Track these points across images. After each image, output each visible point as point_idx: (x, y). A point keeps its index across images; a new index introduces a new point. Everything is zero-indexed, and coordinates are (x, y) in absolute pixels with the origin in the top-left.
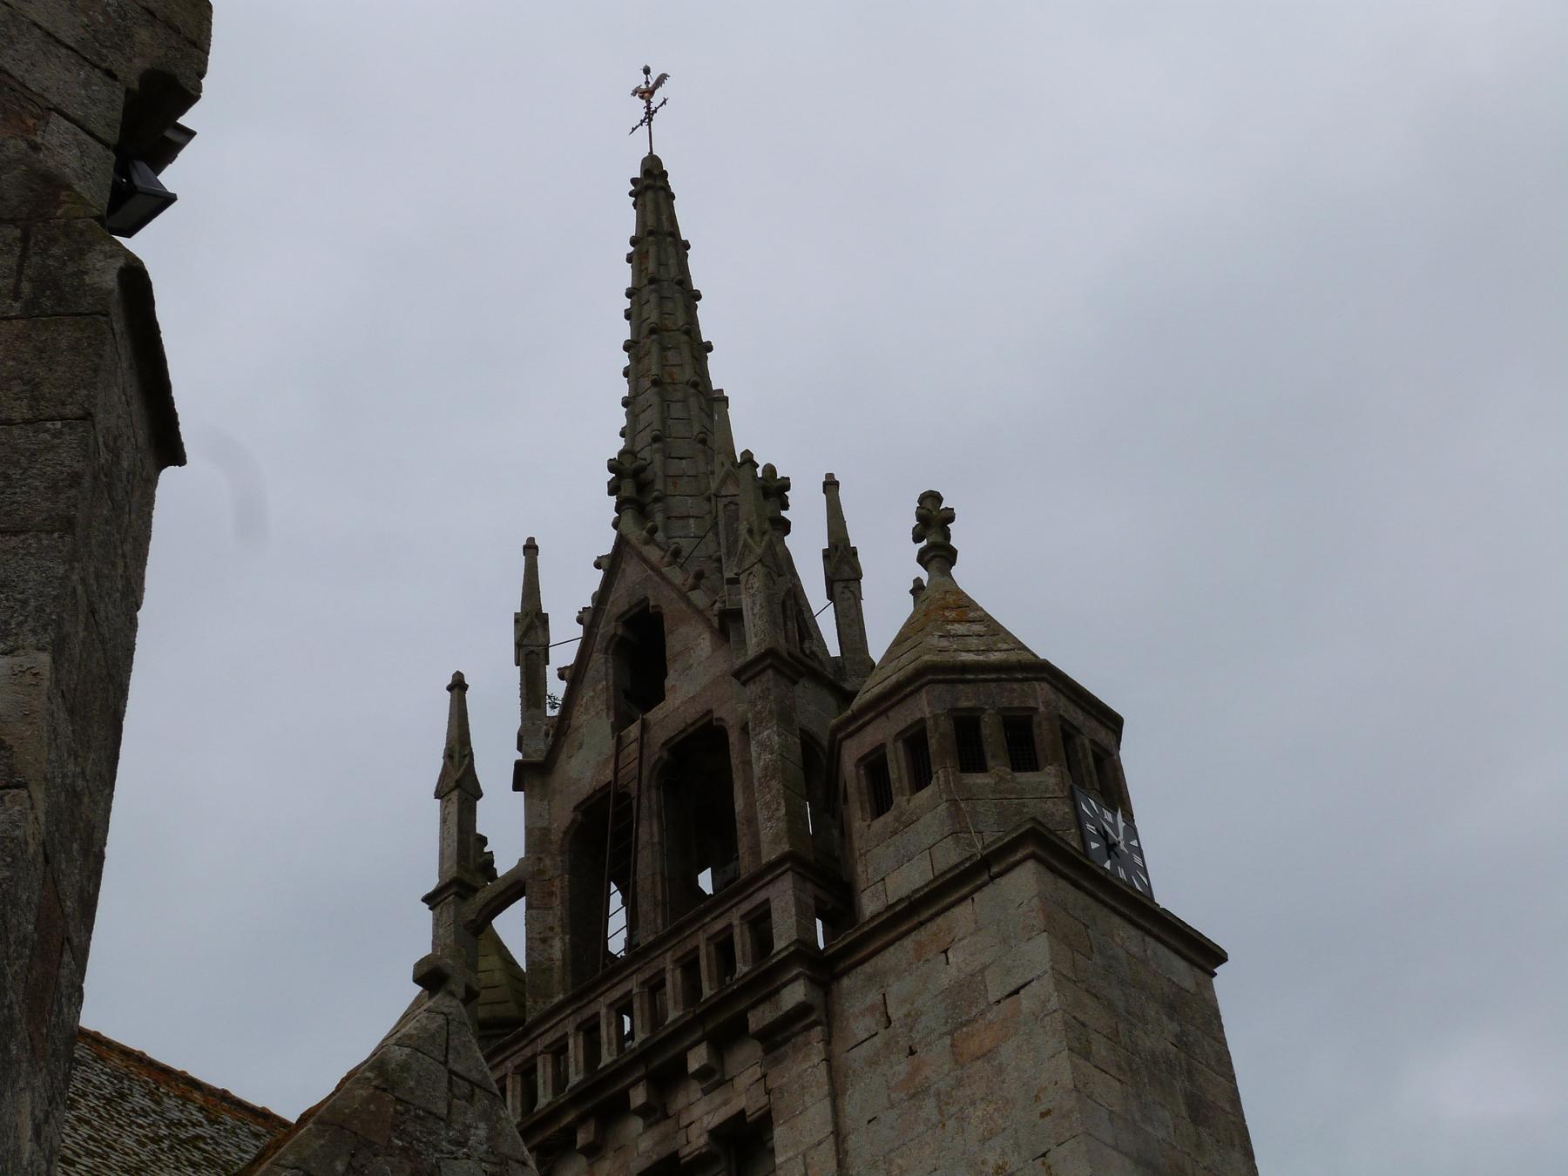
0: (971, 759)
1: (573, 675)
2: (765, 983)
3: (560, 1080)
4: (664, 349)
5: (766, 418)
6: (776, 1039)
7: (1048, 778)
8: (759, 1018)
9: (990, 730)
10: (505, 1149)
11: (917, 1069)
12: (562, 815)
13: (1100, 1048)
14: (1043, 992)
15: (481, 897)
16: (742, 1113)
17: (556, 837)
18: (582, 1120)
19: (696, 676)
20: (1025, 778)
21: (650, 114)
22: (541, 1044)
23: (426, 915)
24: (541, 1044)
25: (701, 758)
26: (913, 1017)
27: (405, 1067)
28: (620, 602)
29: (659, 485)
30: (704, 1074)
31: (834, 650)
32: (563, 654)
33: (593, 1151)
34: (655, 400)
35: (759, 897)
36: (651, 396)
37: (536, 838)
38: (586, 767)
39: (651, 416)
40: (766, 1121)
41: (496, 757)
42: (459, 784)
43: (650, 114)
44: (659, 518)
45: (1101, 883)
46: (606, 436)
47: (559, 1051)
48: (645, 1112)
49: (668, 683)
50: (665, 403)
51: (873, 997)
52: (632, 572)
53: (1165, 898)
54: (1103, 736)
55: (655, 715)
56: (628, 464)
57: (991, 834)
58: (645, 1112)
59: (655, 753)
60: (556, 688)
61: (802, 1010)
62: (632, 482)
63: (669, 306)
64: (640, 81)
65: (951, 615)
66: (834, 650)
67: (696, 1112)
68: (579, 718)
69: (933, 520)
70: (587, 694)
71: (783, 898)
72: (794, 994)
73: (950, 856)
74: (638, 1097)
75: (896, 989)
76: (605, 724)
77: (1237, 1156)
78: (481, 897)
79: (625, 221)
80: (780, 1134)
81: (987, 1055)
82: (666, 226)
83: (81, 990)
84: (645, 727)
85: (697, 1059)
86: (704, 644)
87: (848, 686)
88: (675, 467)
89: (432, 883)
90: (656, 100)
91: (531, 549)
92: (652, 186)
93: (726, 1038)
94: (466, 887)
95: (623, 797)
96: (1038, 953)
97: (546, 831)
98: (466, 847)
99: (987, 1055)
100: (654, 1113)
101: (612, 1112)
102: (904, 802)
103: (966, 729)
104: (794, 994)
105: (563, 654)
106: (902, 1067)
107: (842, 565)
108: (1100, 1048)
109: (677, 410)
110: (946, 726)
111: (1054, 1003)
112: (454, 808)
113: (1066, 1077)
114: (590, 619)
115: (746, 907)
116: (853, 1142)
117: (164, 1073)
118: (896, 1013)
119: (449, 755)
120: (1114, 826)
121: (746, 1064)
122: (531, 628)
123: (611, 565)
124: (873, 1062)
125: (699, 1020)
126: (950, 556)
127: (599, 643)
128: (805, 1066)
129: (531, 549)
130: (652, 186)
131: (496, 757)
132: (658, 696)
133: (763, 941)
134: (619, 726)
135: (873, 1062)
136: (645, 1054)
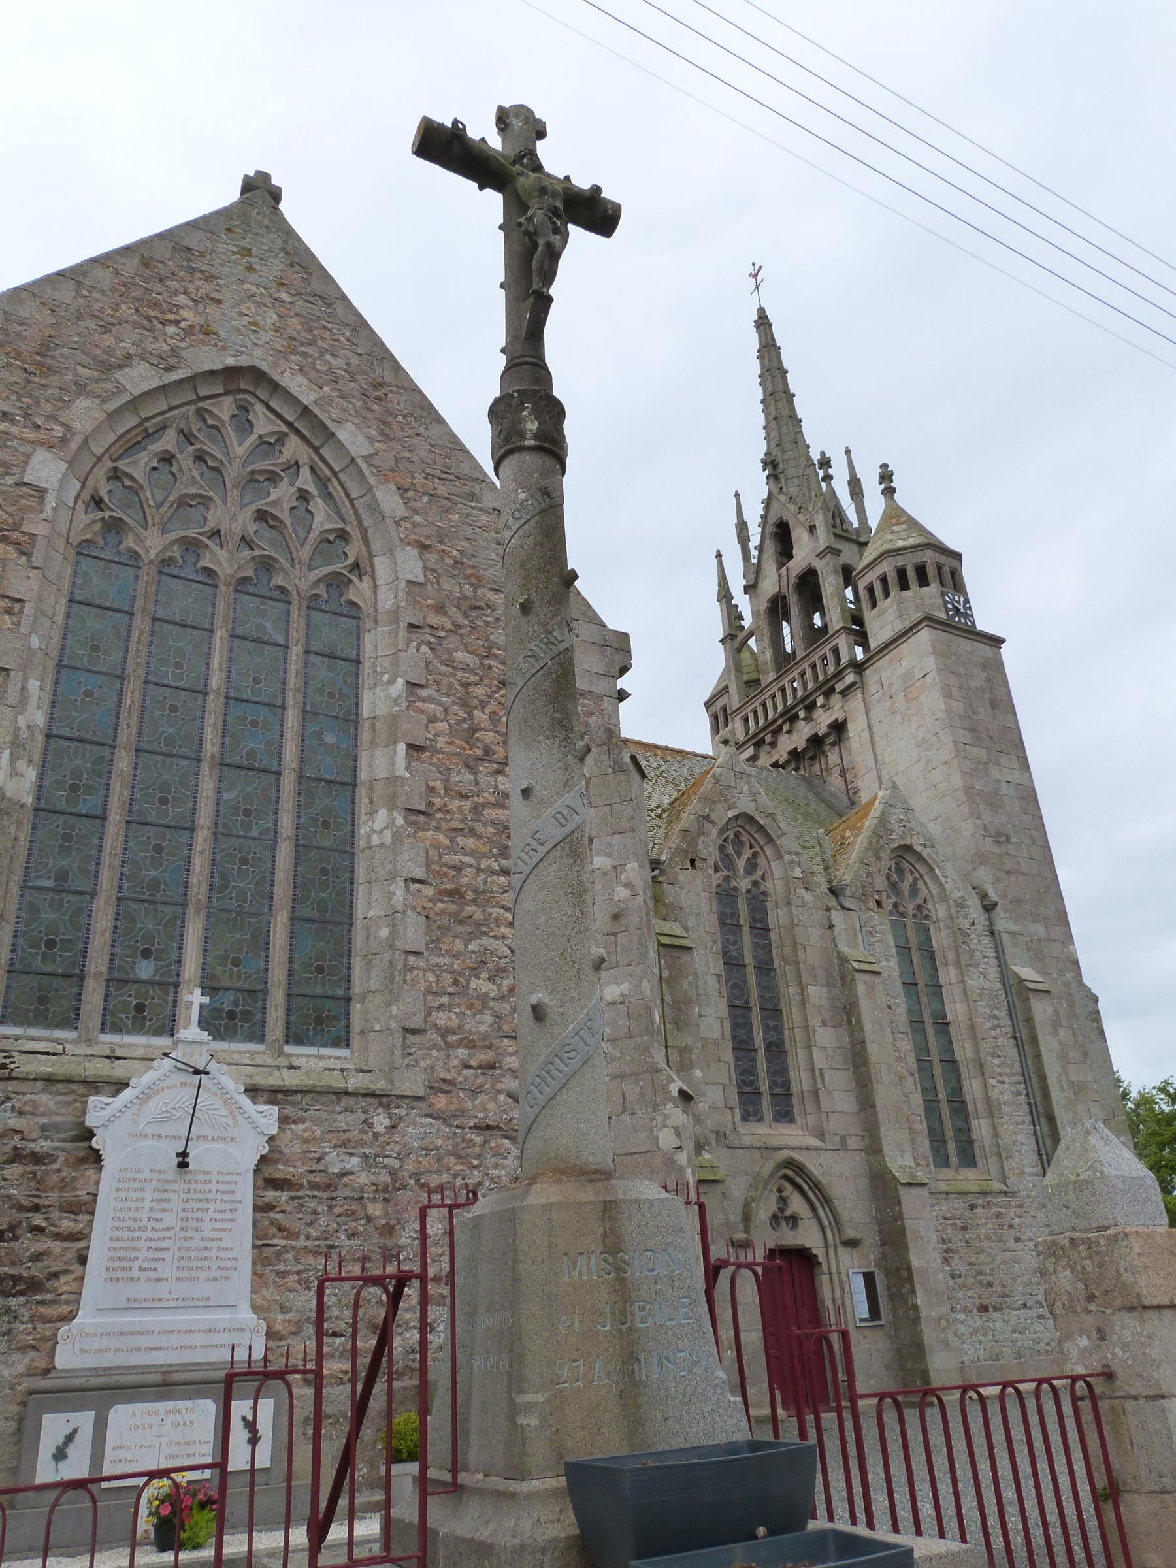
0: (904, 585)
1: (760, 548)
2: (839, 675)
3: (775, 708)
4: (776, 402)
5: (820, 435)
6: (844, 693)
7: (933, 589)
8: (839, 687)
9: (911, 574)
10: (754, 791)
11: (894, 704)
12: (764, 605)
13: (955, 692)
14: (933, 676)
15: (739, 639)
16: (837, 720)
17: (762, 612)
18: (784, 722)
19: (805, 551)
20: (925, 590)
21: (757, 286)
22: (767, 695)
23: (721, 647)
24: (767, 695)
25: (808, 584)
26: (891, 685)
27: (720, 775)
28: (773, 518)
29: (781, 466)
30: (823, 706)
31: (856, 525)
32: (755, 540)
33: (789, 732)
34: (775, 427)
35: (833, 644)
36: (773, 424)
37: (756, 614)
38: (769, 586)
39: (774, 433)
40: (845, 722)
41: (737, 584)
42: (725, 595)
43: (757, 286)
44: (783, 480)
45: (957, 624)
46: (761, 448)
47: (773, 697)
48: (805, 719)
49: (794, 552)
50: (779, 425)
51: (877, 678)
52: (775, 505)
53: (981, 626)
54: (954, 563)
55: (791, 564)
56: (769, 460)
57: (916, 616)
58: (805, 719)
59: (793, 580)
60: (754, 552)
61: (853, 684)
62: (771, 464)
63: (776, 380)
64: (751, 270)
65: (894, 521)
66: (856, 525)
67: (823, 718)
68: (764, 566)
69: (886, 476)
70: (765, 556)
71: (842, 642)
72: (850, 678)
73: (899, 626)
74: (802, 714)
75: (884, 675)
76: (774, 567)
77: (1010, 716)
78: (739, 639)
79: (753, 341)
80: (850, 726)
81: (916, 699)
82: (770, 342)
83: (545, 368)
84: (788, 570)
85: (820, 701)
86: (805, 535)
87: (861, 540)
88: (787, 455)
89: (721, 636)
90: (759, 278)
91: (737, 495)
92: (763, 323)
93: (828, 693)
94: (734, 637)
95: (784, 597)
96: (930, 663)
97: (758, 611)
98: (732, 615)
99: (916, 699)
100: (808, 719)
101: (794, 719)
102: (882, 604)
103: (902, 573)
104: (850, 678)
105: (755, 540)
106: (888, 703)
107: (855, 486)
108: (955, 692)
109: (784, 429)
110: (894, 574)
111: (937, 680)
112: (724, 605)
113: (943, 707)
114: (764, 524)
115: (830, 646)
116: (874, 729)
117: (648, 745)
118: (885, 684)
119: (720, 585)
120: (959, 602)
121: (836, 699)
122: (742, 527)
123: (768, 503)
124: (879, 701)
125: (819, 688)
126: (893, 490)
127: (767, 535)
128: (856, 701)
129: (737, 495)
130: (763, 323)
131: (737, 584)
132: (791, 557)
133: (838, 659)
134: (779, 569)
135: (879, 701)
136: (803, 700)
